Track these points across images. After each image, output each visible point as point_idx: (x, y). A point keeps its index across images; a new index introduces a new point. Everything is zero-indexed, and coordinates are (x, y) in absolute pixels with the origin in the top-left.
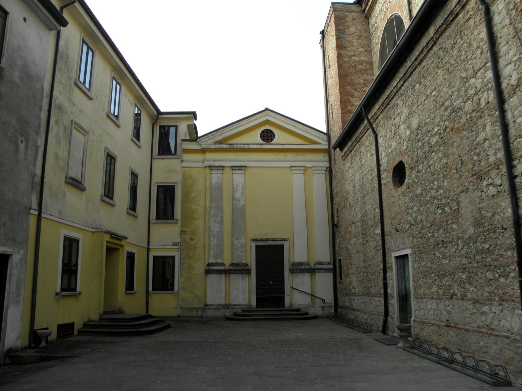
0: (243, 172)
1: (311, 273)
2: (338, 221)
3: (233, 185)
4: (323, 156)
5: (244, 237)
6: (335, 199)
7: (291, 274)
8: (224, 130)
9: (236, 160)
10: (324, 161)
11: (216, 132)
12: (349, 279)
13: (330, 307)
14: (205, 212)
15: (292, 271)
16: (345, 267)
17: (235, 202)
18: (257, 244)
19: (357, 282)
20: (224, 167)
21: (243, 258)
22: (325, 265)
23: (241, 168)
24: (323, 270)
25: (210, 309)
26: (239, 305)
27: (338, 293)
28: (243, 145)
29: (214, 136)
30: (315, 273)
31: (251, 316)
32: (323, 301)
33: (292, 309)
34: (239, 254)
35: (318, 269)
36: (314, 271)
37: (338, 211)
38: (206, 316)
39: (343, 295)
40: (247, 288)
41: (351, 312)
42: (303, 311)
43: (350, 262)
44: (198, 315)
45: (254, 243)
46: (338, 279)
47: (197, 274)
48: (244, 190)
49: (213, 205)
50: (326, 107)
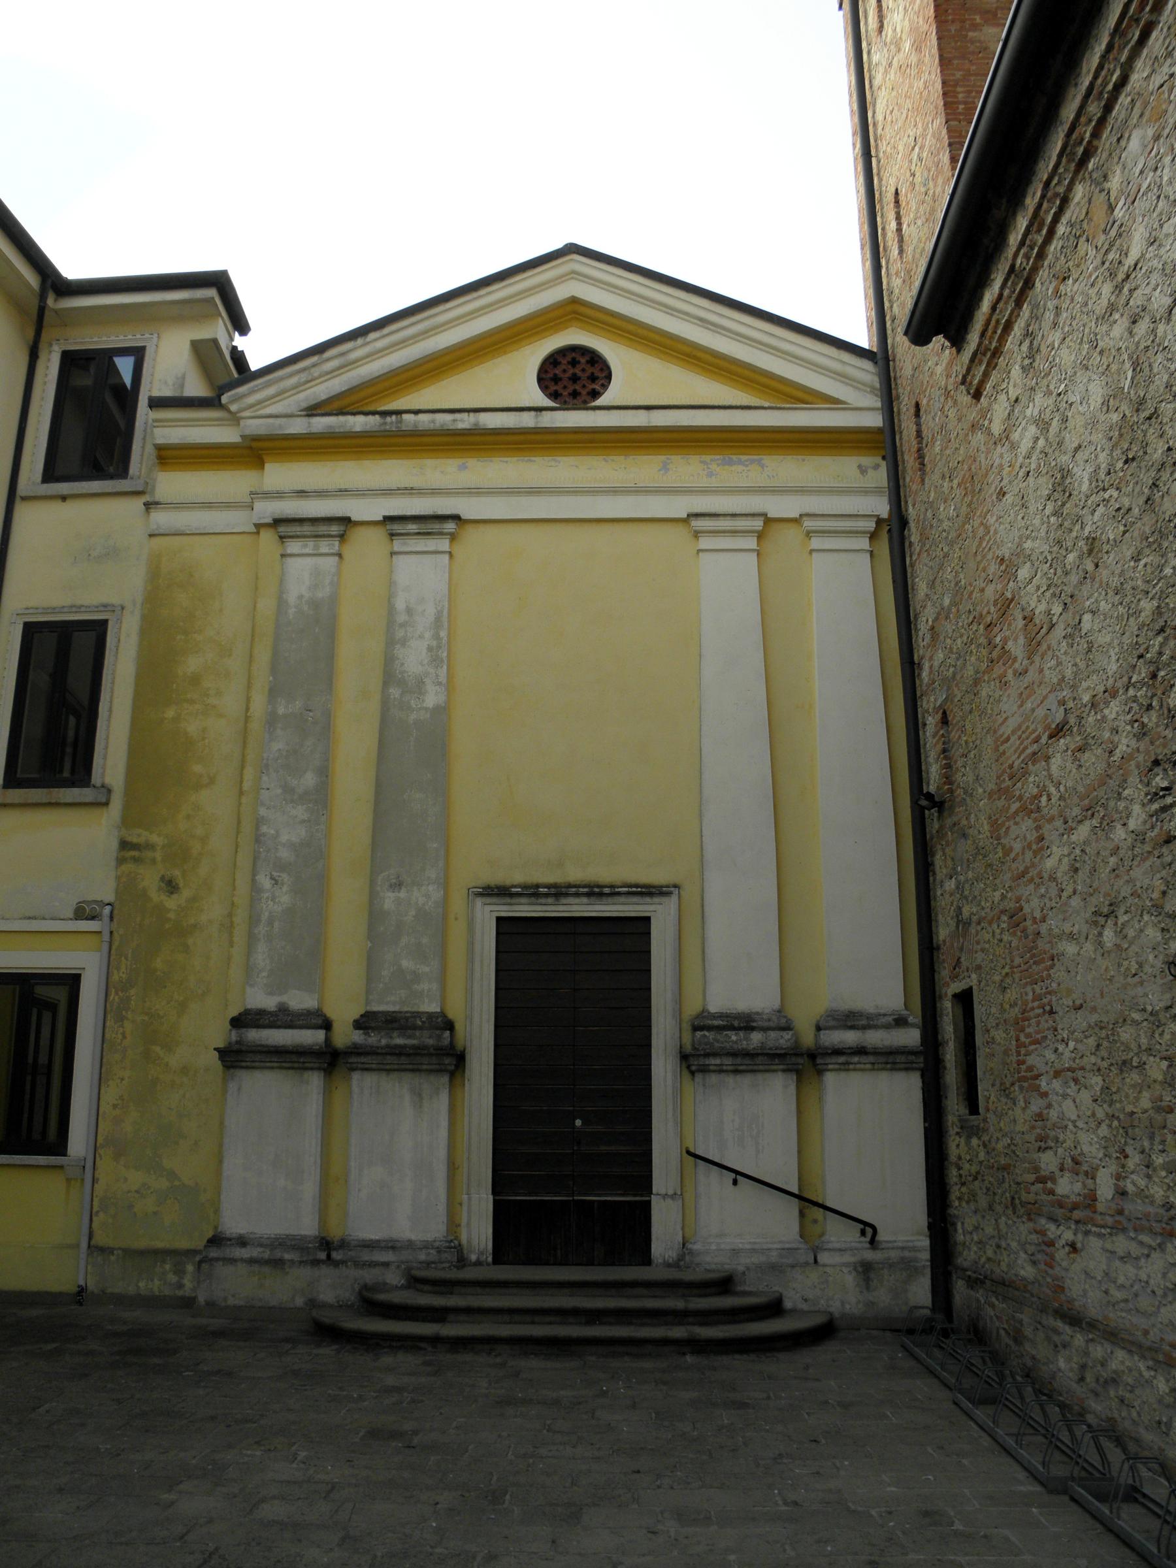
0: (444, 544)
1: (799, 1073)
2: (948, 779)
3: (391, 610)
4: (860, 467)
5: (433, 876)
6: (926, 666)
7: (686, 1073)
8: (358, 349)
9: (409, 491)
10: (865, 492)
11: (315, 359)
12: (1034, 1108)
13: (907, 1266)
14: (245, 743)
15: (692, 1061)
16: (999, 1035)
17: (394, 692)
18: (506, 911)
19: (1104, 1130)
20: (346, 521)
21: (424, 986)
22: (876, 1027)
23: (436, 526)
24: (864, 1059)
25: (233, 1261)
26: (393, 1248)
27: (955, 1192)
28: (448, 417)
29: (303, 377)
30: (820, 1072)
31: (439, 1315)
32: (869, 1231)
33: (688, 1276)
34: (405, 963)
35: (837, 1052)
36: (815, 1065)
37: (945, 721)
38: (210, 1304)
39: (991, 1208)
40: (442, 1153)
41: (1056, 1331)
42: (757, 1289)
43: (1038, 998)
44: (180, 1293)
45: (488, 908)
46: (954, 1106)
47: (185, 1070)
48: (443, 634)
49: (281, 710)
50: (861, 179)
